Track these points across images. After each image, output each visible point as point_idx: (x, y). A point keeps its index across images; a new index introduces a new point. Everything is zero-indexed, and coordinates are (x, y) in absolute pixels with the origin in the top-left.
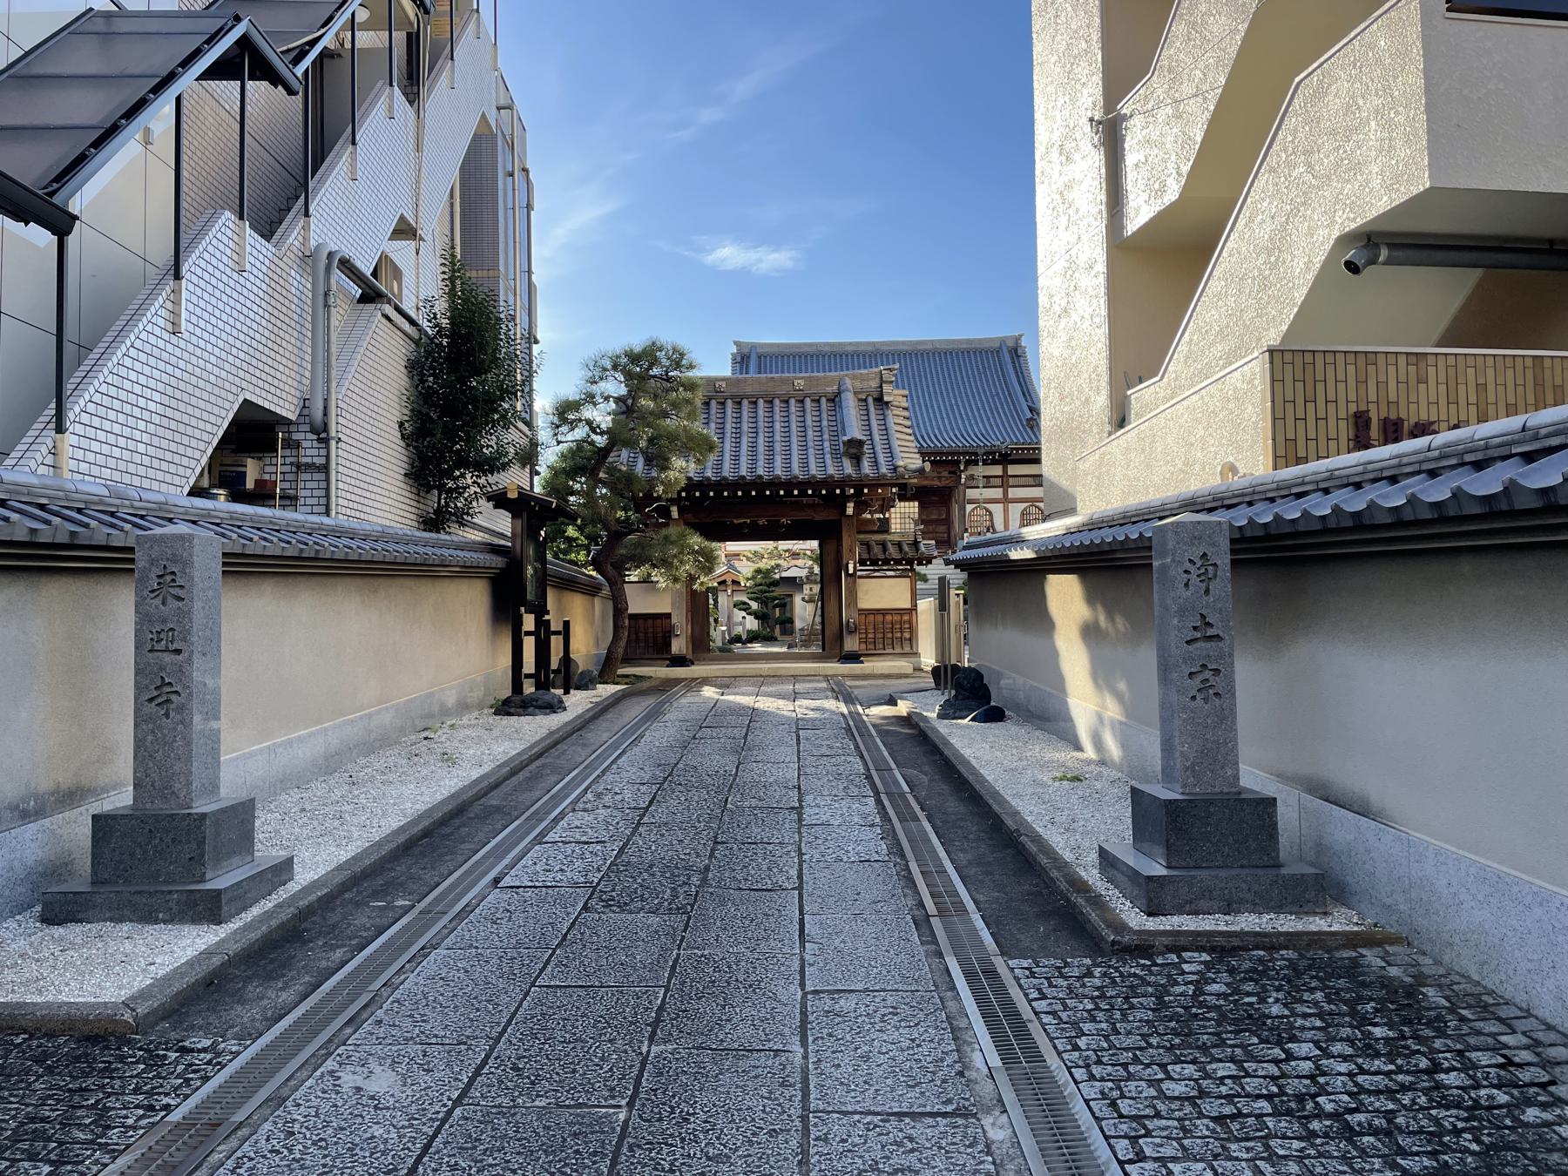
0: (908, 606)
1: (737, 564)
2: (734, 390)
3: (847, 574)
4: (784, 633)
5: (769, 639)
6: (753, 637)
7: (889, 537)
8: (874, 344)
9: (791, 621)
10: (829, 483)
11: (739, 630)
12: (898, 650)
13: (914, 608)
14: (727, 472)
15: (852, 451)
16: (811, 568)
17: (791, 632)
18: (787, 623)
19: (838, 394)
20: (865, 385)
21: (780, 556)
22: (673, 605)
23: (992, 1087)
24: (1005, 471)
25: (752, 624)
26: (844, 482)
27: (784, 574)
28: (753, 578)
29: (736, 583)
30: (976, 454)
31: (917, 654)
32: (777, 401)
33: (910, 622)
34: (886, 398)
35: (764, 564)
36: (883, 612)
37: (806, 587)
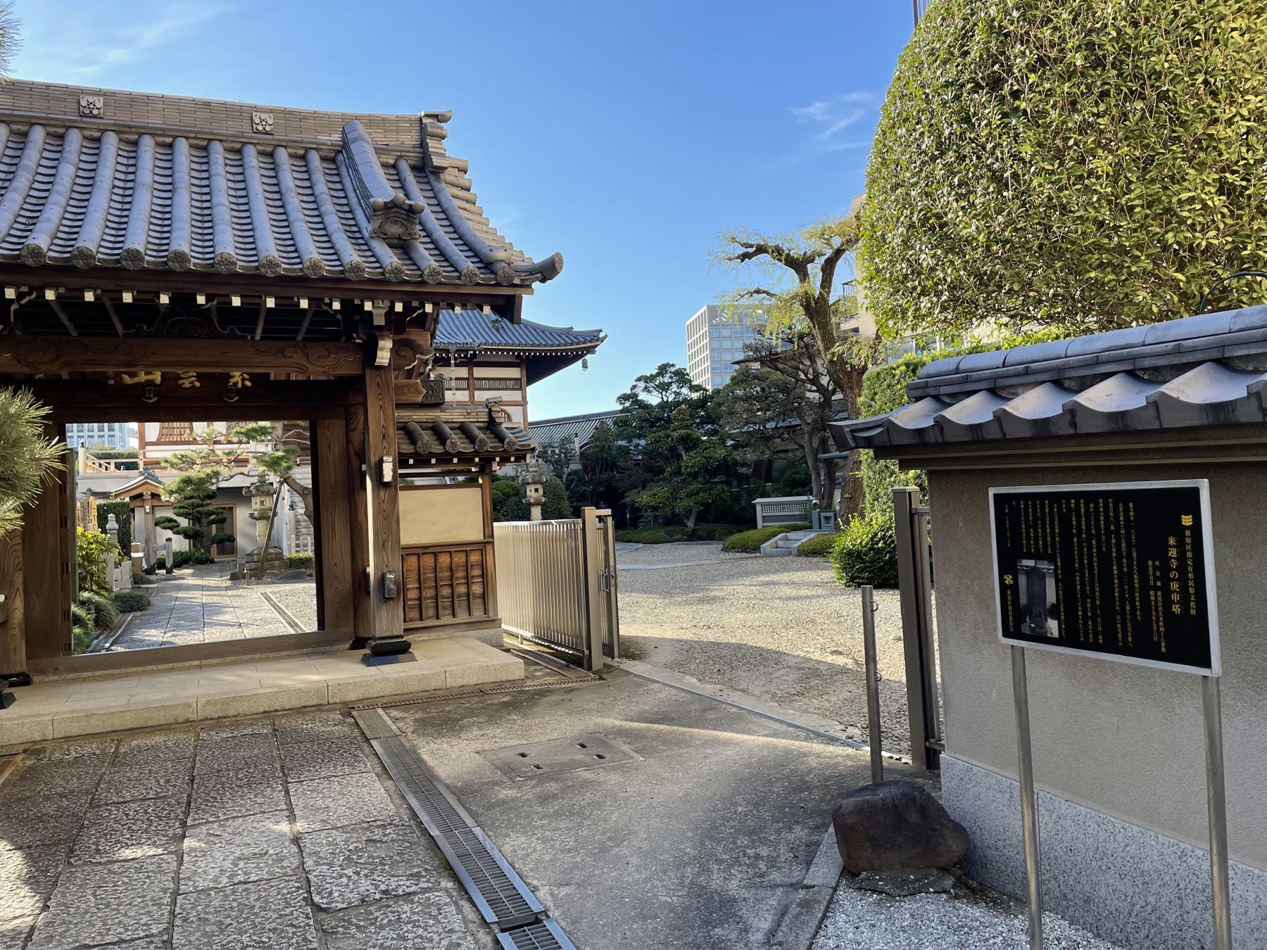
0: (478, 536)
1: (158, 473)
2: (124, 118)
3: (380, 483)
4: (222, 552)
6: (182, 561)
7: (442, 416)
9: (232, 539)
10: (340, 282)
11: (162, 553)
12: (463, 617)
13: (487, 543)
14: (92, 239)
15: (395, 230)
16: (262, 476)
17: (233, 551)
18: (227, 543)
19: (345, 147)
20: (392, 140)
21: (219, 462)
24: (471, 373)
25: (180, 544)
26: (380, 286)
27: (223, 485)
28: (180, 491)
29: (155, 496)
30: (447, 351)
31: (495, 622)
32: (217, 148)
33: (483, 565)
34: (436, 161)
35: (196, 472)
36: (434, 550)
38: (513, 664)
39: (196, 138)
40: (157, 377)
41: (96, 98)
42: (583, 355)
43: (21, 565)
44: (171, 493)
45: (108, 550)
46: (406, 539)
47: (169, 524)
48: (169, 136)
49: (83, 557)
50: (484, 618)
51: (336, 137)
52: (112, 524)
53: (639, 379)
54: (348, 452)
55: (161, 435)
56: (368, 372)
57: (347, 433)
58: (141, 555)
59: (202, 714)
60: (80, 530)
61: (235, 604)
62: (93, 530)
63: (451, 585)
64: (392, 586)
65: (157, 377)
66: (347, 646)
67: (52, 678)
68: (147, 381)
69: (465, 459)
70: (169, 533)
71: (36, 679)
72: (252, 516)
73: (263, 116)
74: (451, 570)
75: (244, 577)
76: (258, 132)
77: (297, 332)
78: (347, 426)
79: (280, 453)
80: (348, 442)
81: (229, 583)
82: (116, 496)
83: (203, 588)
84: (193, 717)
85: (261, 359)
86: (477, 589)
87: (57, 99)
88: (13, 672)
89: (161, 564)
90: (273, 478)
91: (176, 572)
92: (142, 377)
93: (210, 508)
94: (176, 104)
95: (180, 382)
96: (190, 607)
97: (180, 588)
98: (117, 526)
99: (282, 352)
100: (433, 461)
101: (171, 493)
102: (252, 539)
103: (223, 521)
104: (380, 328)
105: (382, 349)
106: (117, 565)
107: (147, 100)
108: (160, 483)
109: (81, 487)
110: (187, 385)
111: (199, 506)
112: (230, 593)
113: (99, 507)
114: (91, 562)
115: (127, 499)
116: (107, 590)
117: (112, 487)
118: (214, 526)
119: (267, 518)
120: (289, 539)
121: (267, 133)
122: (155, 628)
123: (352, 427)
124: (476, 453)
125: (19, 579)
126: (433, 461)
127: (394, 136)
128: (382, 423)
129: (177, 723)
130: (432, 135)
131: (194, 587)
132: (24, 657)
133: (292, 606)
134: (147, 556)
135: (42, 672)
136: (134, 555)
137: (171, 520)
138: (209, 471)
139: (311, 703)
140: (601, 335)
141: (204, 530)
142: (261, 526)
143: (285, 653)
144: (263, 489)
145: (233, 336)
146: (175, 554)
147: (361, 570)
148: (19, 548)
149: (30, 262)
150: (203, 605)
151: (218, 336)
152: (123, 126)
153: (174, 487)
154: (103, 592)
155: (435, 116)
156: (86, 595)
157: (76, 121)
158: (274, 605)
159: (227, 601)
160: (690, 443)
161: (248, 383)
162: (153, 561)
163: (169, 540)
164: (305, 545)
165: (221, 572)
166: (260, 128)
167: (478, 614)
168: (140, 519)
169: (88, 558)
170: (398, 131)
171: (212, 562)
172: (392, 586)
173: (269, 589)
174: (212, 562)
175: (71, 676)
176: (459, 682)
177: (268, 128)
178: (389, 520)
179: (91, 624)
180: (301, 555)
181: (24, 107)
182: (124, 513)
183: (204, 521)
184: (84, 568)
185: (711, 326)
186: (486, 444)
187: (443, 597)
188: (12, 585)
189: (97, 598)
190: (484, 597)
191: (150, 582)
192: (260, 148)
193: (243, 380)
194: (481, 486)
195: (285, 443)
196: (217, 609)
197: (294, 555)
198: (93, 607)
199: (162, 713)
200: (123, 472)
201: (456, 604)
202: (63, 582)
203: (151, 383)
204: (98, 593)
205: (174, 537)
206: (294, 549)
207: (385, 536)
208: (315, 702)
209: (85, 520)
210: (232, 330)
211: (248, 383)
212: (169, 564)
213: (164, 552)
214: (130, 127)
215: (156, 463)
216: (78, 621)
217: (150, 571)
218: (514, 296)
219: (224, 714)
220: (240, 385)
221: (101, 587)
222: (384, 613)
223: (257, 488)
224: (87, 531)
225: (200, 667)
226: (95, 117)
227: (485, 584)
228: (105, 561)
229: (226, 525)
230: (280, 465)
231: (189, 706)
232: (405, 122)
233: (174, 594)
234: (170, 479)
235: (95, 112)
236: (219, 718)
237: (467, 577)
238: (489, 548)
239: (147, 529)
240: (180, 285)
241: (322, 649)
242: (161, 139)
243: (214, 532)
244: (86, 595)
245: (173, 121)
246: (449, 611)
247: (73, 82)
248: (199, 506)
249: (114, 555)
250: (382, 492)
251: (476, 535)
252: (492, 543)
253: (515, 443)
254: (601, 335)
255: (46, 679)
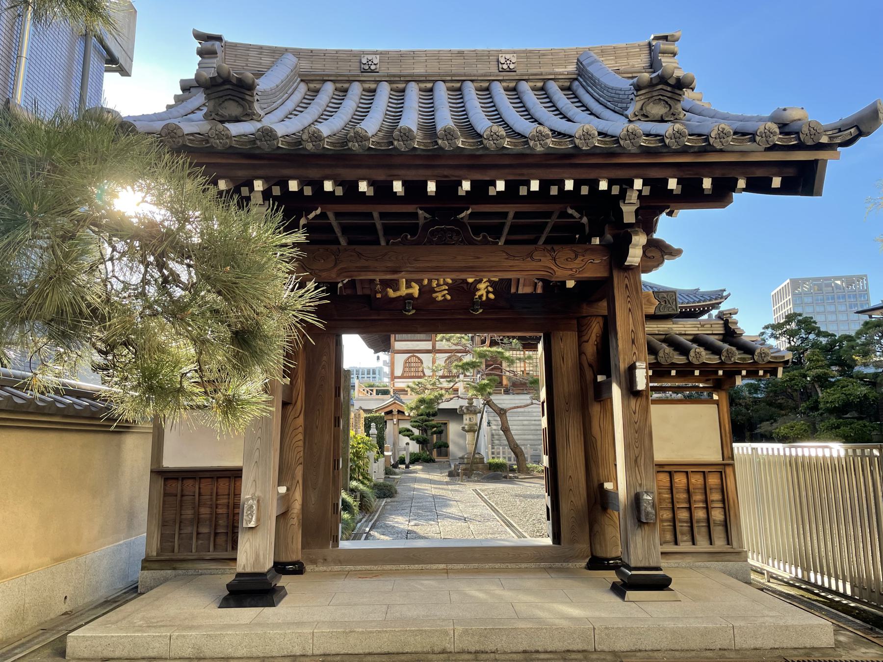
0: (717, 457)
1: (402, 397)
3: (631, 391)
4: (440, 454)
5: (429, 461)
6: (415, 459)
8: (357, 55)
9: (446, 446)
11: (403, 453)
12: (703, 545)
17: (446, 454)
18: (443, 449)
22: (248, 456)
23: (685, 480)
25: (414, 447)
29: (400, 412)
31: (740, 555)
33: (723, 490)
35: (427, 395)
37: (466, 417)
38: (819, 626)
39: (452, 81)
40: (415, 290)
41: (374, 56)
42: (708, 311)
43: (302, 460)
44: (412, 409)
45: (370, 449)
46: (660, 456)
47: (407, 433)
48: (430, 81)
49: (353, 454)
50: (727, 548)
51: (572, 68)
52: (373, 431)
53: (767, 327)
54: (581, 364)
55: (404, 371)
56: (615, 274)
57: (580, 345)
58: (390, 453)
59: (459, 646)
60: (352, 433)
61: (457, 498)
62: (361, 433)
63: (690, 509)
64: (650, 509)
65: (415, 290)
66: (584, 564)
67: (322, 568)
68: (407, 294)
69: (707, 371)
70: (407, 440)
71: (309, 568)
72: (463, 428)
73: (508, 56)
74: (688, 491)
75: (458, 475)
76: (504, 70)
77: (555, 228)
78: (580, 337)
79: (486, 382)
80: (581, 353)
81: (447, 479)
82: (376, 411)
83: (431, 482)
84: (450, 647)
85: (511, 263)
86: (717, 515)
87: (344, 60)
88: (290, 560)
89: (402, 461)
90: (479, 402)
91: (412, 467)
92: (403, 291)
93: (433, 423)
94: (437, 56)
95: (434, 295)
96: (423, 497)
97: (416, 480)
98: (376, 432)
99: (530, 255)
100: (673, 373)
101: (412, 409)
102: (463, 448)
103: (441, 432)
104: (630, 225)
105: (636, 245)
106: (376, 460)
107: (414, 55)
108: (403, 403)
109: (356, 405)
110: (440, 298)
111: (426, 421)
112: (450, 487)
113: (366, 419)
114: (359, 458)
115: (383, 414)
116: (369, 480)
117: (373, 406)
118: (435, 436)
119: (474, 431)
120: (487, 448)
121: (511, 71)
122: (402, 515)
123: (585, 338)
124: (722, 364)
125: (299, 472)
126: (673, 373)
127: (625, 61)
128: (631, 327)
129: (433, 653)
130: (664, 52)
131: (426, 481)
132: (300, 547)
133: (517, 515)
134: (394, 454)
135: (314, 562)
136: (386, 453)
137: (408, 430)
138: (436, 394)
139: (575, 647)
140: (725, 294)
141: (429, 438)
142: (469, 436)
143: (523, 566)
144: (471, 410)
145: (485, 242)
146: (411, 454)
147: (596, 484)
148: (301, 443)
149: (310, 146)
150: (434, 497)
151: (471, 242)
152: (394, 76)
153: (413, 405)
154: (366, 482)
155: (665, 38)
156: (354, 484)
157: (358, 76)
158: (485, 501)
159: (449, 495)
160: (823, 381)
161: (492, 296)
162: (397, 459)
163: (408, 444)
164: (498, 453)
165: (441, 469)
166: (505, 67)
167: (720, 543)
168: (390, 429)
169: (357, 455)
170: (628, 56)
171: (434, 461)
172: (650, 509)
173: (479, 486)
174: (434, 461)
175: (337, 568)
176: (751, 643)
177: (512, 66)
178: (640, 436)
179: (356, 509)
180: (496, 460)
181: (318, 67)
182: (381, 423)
183: (429, 432)
184: (354, 461)
185: (794, 295)
186: (733, 354)
187: (681, 521)
188: (293, 478)
189: (361, 487)
190: (726, 525)
191: (395, 474)
192: (505, 84)
193: (488, 292)
194: (717, 403)
195: (487, 375)
196: (444, 502)
197: (491, 460)
198: (358, 494)
199: (418, 638)
200: (380, 396)
201: (696, 530)
202: (334, 476)
203: (410, 296)
204: (362, 483)
205: (411, 442)
206: (490, 456)
207: (637, 451)
208: (580, 647)
209: (356, 427)
210: (484, 237)
211: (492, 296)
212: (407, 461)
213: (404, 452)
214: (400, 76)
215: (403, 391)
216: (347, 507)
217: (395, 466)
218: (815, 162)
219: (482, 648)
220: (484, 298)
221: (365, 478)
222: (639, 539)
223: (467, 408)
224: (357, 434)
225: (447, 571)
226: (373, 71)
227: (726, 509)
228: (368, 458)
229: (443, 435)
230: (485, 390)
231: (446, 633)
232: (634, 47)
233: (412, 485)
234: (410, 400)
235: (373, 67)
236: (477, 652)
237: (706, 501)
238: (729, 470)
239: (394, 435)
240: (446, 172)
241: (558, 565)
242: (423, 85)
243: (435, 440)
244: (354, 484)
245: (433, 68)
246: (687, 537)
247: (356, 47)
248: (426, 421)
249: (373, 454)
250: (633, 402)
251: (714, 455)
252: (733, 465)
253: (766, 355)
254: (725, 294)
255: (317, 569)
